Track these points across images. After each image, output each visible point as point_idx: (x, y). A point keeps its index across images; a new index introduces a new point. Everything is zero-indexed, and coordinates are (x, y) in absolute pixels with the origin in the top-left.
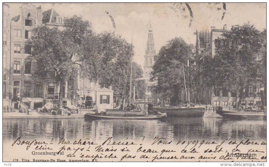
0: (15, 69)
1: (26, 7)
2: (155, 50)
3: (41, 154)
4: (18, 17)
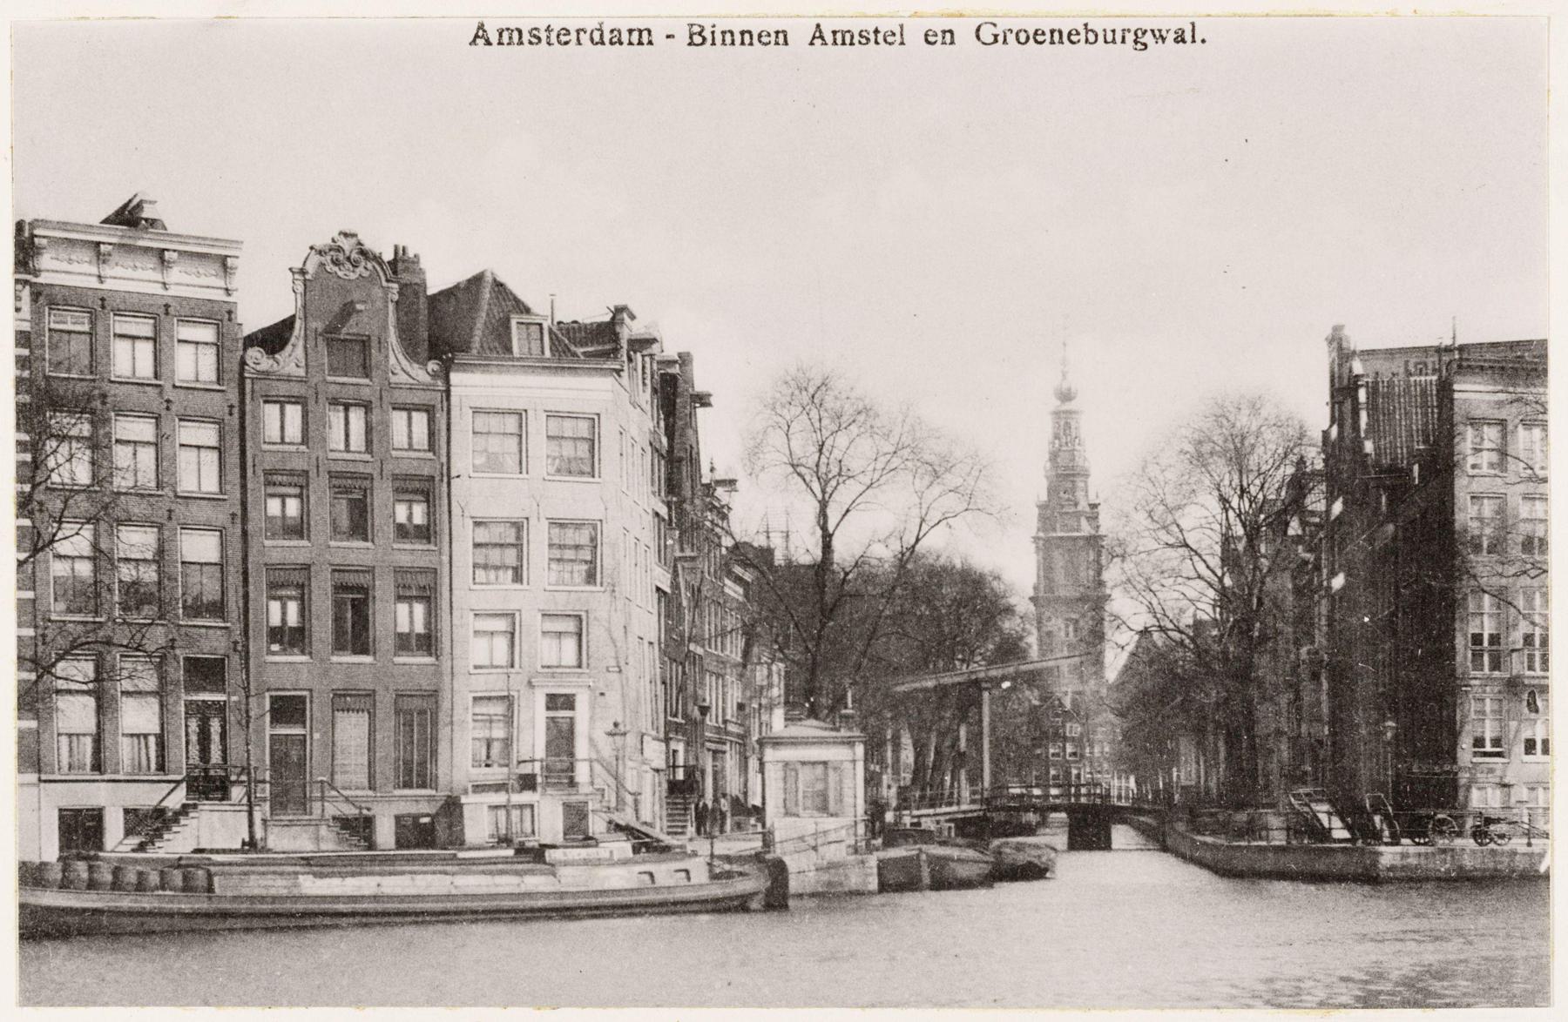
0: (275, 620)
1: (330, 267)
2: (1093, 500)
3: (1040, 38)
4: (288, 324)
